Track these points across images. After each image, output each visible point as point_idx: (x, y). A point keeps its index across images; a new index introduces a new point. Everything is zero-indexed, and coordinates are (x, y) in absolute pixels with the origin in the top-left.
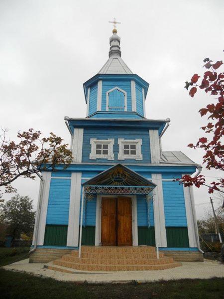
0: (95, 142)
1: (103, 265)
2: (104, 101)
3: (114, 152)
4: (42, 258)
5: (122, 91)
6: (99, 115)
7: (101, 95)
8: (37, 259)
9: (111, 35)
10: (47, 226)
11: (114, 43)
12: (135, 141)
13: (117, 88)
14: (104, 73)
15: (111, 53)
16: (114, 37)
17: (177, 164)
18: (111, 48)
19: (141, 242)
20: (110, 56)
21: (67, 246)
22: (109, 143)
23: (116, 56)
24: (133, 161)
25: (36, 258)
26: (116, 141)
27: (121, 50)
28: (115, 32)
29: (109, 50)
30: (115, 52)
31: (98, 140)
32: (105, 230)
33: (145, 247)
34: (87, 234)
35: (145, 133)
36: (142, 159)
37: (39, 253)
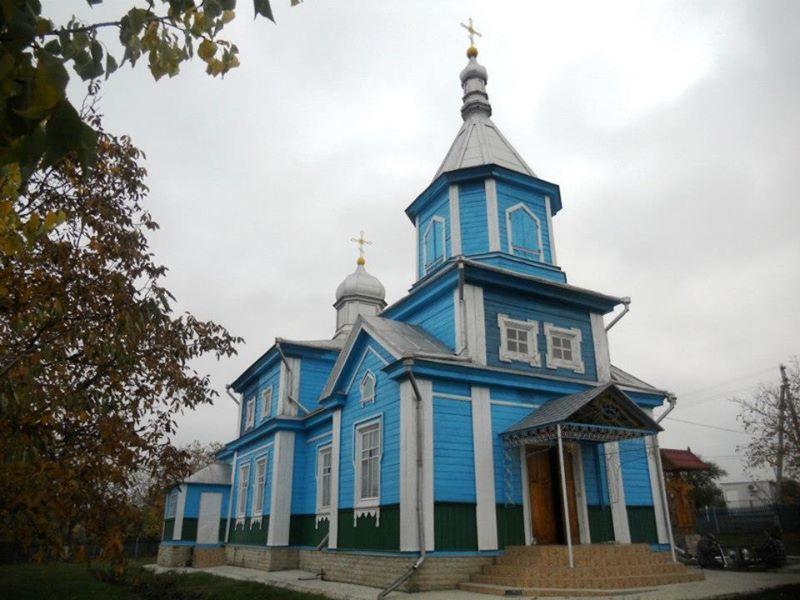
0: (506, 324)
1: (624, 577)
2: (503, 230)
3: (540, 350)
4: (437, 580)
5: (533, 215)
6: (503, 261)
7: (458, 232)
8: (428, 582)
9: (464, 63)
10: (438, 505)
11: (474, 85)
12: (525, 323)
13: (521, 204)
14: (457, 167)
15: (467, 112)
16: (473, 67)
17: (638, 388)
18: (465, 99)
19: (595, 539)
20: (465, 119)
21: (480, 548)
22: (529, 328)
23: (476, 118)
24: (525, 368)
25: (425, 580)
26: (541, 327)
27: (491, 101)
28: (472, 54)
29: (461, 104)
30: (476, 107)
31: (510, 320)
32: (537, 514)
33: (643, 547)
34: (454, 520)
35: (582, 317)
36: (583, 372)
37: (428, 567)
